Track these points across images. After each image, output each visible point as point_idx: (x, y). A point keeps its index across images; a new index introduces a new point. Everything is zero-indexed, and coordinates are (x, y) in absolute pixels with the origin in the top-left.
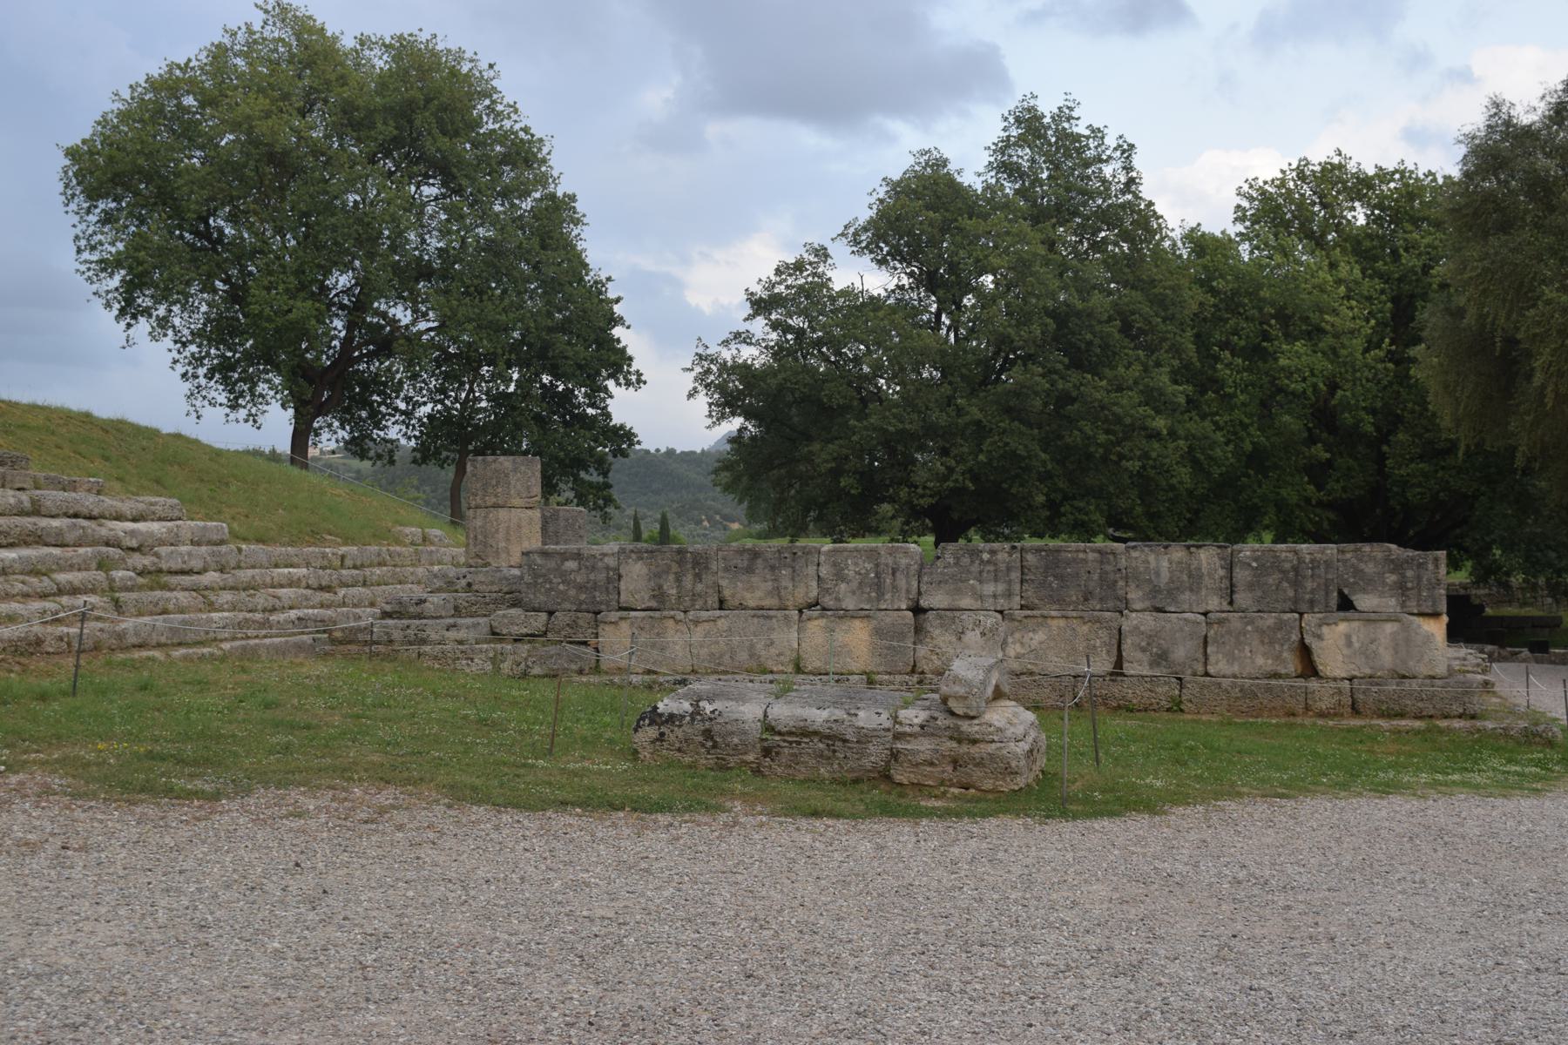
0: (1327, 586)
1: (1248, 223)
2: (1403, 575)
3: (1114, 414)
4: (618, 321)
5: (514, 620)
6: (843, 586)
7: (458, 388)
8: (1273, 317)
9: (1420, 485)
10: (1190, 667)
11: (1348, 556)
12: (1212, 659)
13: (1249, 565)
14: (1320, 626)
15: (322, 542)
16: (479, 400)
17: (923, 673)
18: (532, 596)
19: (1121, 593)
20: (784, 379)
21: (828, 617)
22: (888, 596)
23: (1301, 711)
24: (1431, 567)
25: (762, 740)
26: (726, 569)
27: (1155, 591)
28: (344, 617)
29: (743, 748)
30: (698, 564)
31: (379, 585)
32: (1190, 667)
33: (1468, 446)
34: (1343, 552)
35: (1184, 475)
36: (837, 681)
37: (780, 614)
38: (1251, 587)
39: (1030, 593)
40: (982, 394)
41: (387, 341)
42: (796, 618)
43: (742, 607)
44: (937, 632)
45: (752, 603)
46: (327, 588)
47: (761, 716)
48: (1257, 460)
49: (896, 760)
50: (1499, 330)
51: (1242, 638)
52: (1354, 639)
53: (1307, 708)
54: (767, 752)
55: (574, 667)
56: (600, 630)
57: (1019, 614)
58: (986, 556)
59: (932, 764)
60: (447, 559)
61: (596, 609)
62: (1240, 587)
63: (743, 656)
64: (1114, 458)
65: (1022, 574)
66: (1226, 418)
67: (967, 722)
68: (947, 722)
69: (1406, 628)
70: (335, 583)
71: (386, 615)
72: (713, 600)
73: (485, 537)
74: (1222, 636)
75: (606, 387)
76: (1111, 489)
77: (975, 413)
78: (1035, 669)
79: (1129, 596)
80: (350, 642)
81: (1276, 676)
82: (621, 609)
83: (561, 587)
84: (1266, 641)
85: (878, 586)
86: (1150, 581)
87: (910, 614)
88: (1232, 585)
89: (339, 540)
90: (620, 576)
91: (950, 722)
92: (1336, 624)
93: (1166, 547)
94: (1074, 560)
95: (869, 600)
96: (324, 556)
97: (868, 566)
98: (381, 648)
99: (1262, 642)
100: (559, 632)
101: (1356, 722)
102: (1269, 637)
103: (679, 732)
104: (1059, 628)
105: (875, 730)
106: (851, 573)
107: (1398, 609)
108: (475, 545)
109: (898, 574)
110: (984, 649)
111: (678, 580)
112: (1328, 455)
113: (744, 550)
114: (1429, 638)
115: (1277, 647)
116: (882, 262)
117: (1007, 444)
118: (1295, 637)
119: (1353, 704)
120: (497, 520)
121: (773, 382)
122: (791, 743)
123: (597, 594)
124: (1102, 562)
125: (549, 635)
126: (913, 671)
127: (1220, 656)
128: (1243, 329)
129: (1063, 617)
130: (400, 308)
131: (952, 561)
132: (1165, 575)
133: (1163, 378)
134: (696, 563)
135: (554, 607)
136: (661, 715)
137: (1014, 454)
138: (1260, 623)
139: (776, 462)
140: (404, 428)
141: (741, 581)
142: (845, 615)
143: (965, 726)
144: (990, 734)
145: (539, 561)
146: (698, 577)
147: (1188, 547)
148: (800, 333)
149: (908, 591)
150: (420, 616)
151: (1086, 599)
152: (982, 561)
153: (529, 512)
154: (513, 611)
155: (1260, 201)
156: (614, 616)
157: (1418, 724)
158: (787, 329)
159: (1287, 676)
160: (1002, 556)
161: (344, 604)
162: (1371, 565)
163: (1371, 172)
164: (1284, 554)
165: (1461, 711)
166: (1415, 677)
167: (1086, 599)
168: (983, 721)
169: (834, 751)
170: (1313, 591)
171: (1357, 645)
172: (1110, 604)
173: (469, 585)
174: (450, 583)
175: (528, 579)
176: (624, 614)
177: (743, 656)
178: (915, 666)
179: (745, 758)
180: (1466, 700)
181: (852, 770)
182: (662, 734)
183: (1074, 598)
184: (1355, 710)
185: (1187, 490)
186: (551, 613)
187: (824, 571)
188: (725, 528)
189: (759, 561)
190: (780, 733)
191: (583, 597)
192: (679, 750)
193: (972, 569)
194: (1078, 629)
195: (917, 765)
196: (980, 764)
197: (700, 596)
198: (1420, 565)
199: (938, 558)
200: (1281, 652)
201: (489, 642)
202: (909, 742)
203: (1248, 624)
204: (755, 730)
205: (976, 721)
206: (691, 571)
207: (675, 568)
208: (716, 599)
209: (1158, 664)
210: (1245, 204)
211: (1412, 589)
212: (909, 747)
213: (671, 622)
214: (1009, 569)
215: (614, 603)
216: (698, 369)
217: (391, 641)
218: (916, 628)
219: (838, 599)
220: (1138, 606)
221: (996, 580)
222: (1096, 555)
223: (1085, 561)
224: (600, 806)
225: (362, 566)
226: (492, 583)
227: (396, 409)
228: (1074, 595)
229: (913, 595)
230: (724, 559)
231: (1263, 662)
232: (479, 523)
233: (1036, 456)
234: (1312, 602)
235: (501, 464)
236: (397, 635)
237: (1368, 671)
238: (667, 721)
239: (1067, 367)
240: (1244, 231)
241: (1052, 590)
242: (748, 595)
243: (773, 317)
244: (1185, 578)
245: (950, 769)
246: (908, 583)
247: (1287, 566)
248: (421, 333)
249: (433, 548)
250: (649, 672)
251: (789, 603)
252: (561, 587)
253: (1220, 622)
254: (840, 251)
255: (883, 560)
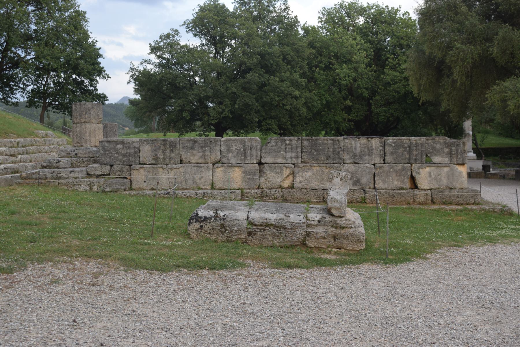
0: (421, 153)
1: (323, 23)
2: (451, 149)
3: (281, 90)
4: (100, 56)
5: (96, 168)
6: (230, 154)
7: (42, 80)
8: (333, 56)
9: (383, 115)
10: (368, 185)
11: (430, 141)
12: (377, 182)
13: (391, 145)
14: (419, 169)
15: (8, 137)
16: (50, 84)
17: (262, 188)
18: (104, 159)
19: (341, 156)
20: (162, 76)
21: (224, 167)
22: (249, 158)
23: (412, 202)
24: (462, 146)
25: (247, 228)
26: (183, 148)
27: (355, 155)
28: (28, 168)
29: (240, 232)
30: (172, 145)
31: (32, 154)
32: (368, 185)
33: (423, 100)
34: (428, 140)
35: (304, 110)
36: (231, 193)
37: (205, 165)
38: (392, 154)
39: (305, 157)
40: (236, 82)
41: (16, 63)
42: (212, 167)
43: (190, 163)
44: (268, 172)
45: (194, 161)
46: (13, 155)
47: (246, 217)
48: (328, 106)
49: (308, 237)
50: (437, 58)
51: (389, 174)
52: (432, 174)
53: (414, 201)
54: (250, 234)
55: (123, 188)
56: (132, 172)
57: (301, 165)
58: (288, 142)
59: (324, 238)
60: (55, 143)
61: (130, 164)
62: (388, 154)
63: (190, 182)
64: (281, 105)
65: (302, 149)
66: (317, 91)
67: (340, 219)
68: (330, 219)
69: (452, 169)
70: (16, 153)
71: (44, 167)
72: (178, 160)
73: (81, 135)
74: (381, 173)
75: (96, 80)
76: (281, 115)
77: (234, 89)
78: (307, 187)
79: (344, 158)
80: (29, 179)
81: (402, 189)
82: (140, 164)
83: (116, 155)
84: (398, 175)
85: (245, 154)
86: (353, 151)
87: (257, 165)
88: (384, 153)
89: (16, 136)
90: (140, 151)
91: (332, 219)
92: (425, 168)
93: (359, 138)
94: (323, 143)
95: (241, 160)
96: (11, 142)
97: (241, 146)
98: (43, 181)
99: (397, 176)
100: (115, 173)
101: (435, 207)
102: (399, 173)
103: (209, 225)
104: (317, 170)
105: (299, 223)
106: (234, 149)
107: (449, 162)
108: (77, 138)
109: (252, 149)
110: (341, 186)
111: (164, 152)
112: (351, 104)
113: (191, 140)
114: (461, 173)
115: (402, 177)
116: (195, 35)
117: (245, 100)
118: (409, 173)
119: (432, 199)
120: (86, 128)
121: (158, 78)
122: (261, 229)
123: (131, 158)
124: (334, 144)
125: (111, 175)
126: (258, 188)
127: (380, 181)
128: (323, 61)
129: (319, 166)
130: (20, 51)
131: (274, 144)
132: (358, 149)
133: (297, 76)
134: (171, 145)
135: (113, 164)
136: (201, 217)
137: (247, 104)
138: (395, 168)
139: (159, 106)
140: (22, 93)
141: (189, 153)
142: (231, 166)
143: (338, 221)
144: (350, 224)
145: (106, 145)
146: (172, 151)
147: (368, 138)
148: (168, 60)
149: (257, 156)
150: (58, 168)
151: (327, 159)
152: (286, 144)
153: (98, 125)
154: (95, 165)
155: (327, 15)
156: (138, 167)
157: (459, 207)
158: (164, 59)
159: (406, 189)
160: (294, 142)
161: (20, 162)
162: (438, 145)
163: (365, 5)
164: (405, 141)
165: (474, 202)
166: (455, 189)
167: (327, 159)
168: (346, 218)
169: (281, 233)
170: (416, 155)
171: (433, 176)
172: (337, 161)
173: (76, 154)
174: (68, 154)
175: (102, 152)
176: (142, 166)
177: (190, 182)
178: (259, 186)
179: (239, 236)
180: (476, 197)
181: (289, 241)
182: (202, 226)
183: (323, 158)
184: (433, 202)
185: (305, 116)
186: (111, 166)
187: (223, 148)
188: (123, 129)
189: (197, 145)
190: (255, 225)
191: (125, 159)
192: (209, 233)
193: (282, 147)
194: (324, 171)
195: (318, 239)
196: (346, 238)
197: (173, 158)
198: (457, 145)
199: (269, 143)
200: (404, 179)
201: (86, 178)
202: (313, 228)
203: (391, 168)
204: (244, 224)
205: (343, 219)
206: (169, 149)
207: (162, 147)
208: (179, 160)
209: (356, 185)
210: (321, 16)
211: (454, 154)
212: (314, 231)
213: (161, 169)
214: (297, 147)
215: (138, 162)
216: (131, 74)
217: (46, 178)
218: (259, 170)
219: (228, 159)
220: (348, 162)
221: (292, 151)
222: (332, 141)
223: (327, 144)
224: (194, 267)
225: (25, 146)
226: (86, 154)
227: (19, 87)
228: (322, 157)
229: (259, 158)
230: (182, 144)
231: (397, 183)
232: (78, 129)
233: (255, 104)
234: (416, 160)
235: (87, 105)
236: (49, 175)
237: (437, 186)
238: (204, 220)
239: (264, 73)
240: (321, 26)
241: (314, 155)
242: (192, 158)
243: (158, 54)
244: (366, 150)
245: (332, 240)
246: (257, 153)
247: (406, 145)
248: (28, 60)
249: (50, 139)
250: (152, 189)
251: (209, 161)
252: (116, 155)
253: (380, 168)
254: (183, 30)
255: (247, 144)
